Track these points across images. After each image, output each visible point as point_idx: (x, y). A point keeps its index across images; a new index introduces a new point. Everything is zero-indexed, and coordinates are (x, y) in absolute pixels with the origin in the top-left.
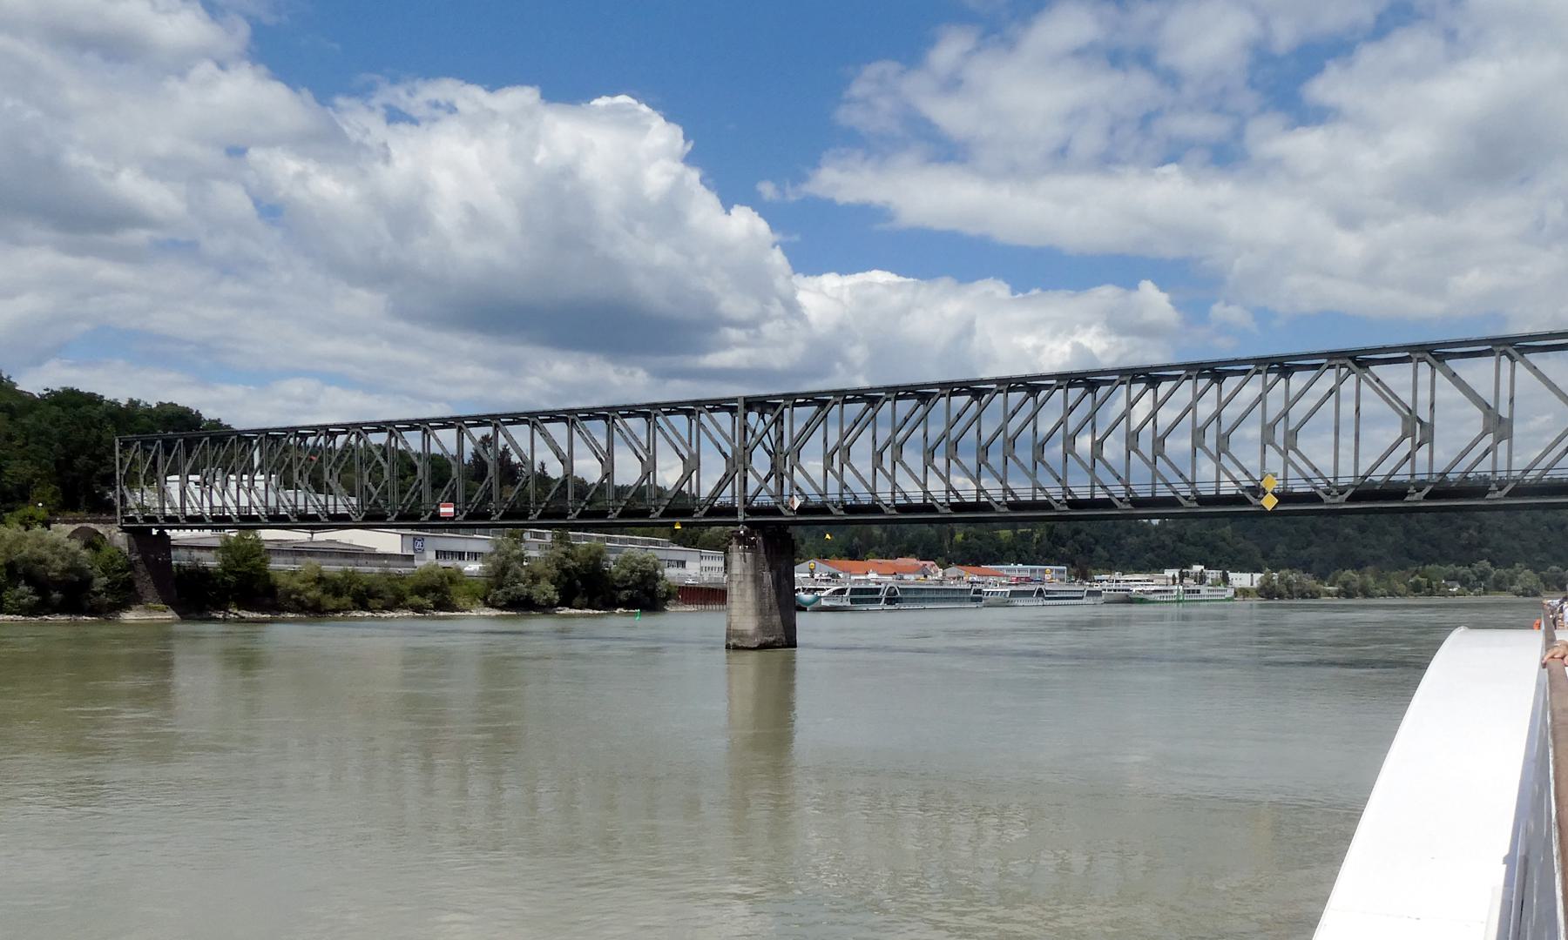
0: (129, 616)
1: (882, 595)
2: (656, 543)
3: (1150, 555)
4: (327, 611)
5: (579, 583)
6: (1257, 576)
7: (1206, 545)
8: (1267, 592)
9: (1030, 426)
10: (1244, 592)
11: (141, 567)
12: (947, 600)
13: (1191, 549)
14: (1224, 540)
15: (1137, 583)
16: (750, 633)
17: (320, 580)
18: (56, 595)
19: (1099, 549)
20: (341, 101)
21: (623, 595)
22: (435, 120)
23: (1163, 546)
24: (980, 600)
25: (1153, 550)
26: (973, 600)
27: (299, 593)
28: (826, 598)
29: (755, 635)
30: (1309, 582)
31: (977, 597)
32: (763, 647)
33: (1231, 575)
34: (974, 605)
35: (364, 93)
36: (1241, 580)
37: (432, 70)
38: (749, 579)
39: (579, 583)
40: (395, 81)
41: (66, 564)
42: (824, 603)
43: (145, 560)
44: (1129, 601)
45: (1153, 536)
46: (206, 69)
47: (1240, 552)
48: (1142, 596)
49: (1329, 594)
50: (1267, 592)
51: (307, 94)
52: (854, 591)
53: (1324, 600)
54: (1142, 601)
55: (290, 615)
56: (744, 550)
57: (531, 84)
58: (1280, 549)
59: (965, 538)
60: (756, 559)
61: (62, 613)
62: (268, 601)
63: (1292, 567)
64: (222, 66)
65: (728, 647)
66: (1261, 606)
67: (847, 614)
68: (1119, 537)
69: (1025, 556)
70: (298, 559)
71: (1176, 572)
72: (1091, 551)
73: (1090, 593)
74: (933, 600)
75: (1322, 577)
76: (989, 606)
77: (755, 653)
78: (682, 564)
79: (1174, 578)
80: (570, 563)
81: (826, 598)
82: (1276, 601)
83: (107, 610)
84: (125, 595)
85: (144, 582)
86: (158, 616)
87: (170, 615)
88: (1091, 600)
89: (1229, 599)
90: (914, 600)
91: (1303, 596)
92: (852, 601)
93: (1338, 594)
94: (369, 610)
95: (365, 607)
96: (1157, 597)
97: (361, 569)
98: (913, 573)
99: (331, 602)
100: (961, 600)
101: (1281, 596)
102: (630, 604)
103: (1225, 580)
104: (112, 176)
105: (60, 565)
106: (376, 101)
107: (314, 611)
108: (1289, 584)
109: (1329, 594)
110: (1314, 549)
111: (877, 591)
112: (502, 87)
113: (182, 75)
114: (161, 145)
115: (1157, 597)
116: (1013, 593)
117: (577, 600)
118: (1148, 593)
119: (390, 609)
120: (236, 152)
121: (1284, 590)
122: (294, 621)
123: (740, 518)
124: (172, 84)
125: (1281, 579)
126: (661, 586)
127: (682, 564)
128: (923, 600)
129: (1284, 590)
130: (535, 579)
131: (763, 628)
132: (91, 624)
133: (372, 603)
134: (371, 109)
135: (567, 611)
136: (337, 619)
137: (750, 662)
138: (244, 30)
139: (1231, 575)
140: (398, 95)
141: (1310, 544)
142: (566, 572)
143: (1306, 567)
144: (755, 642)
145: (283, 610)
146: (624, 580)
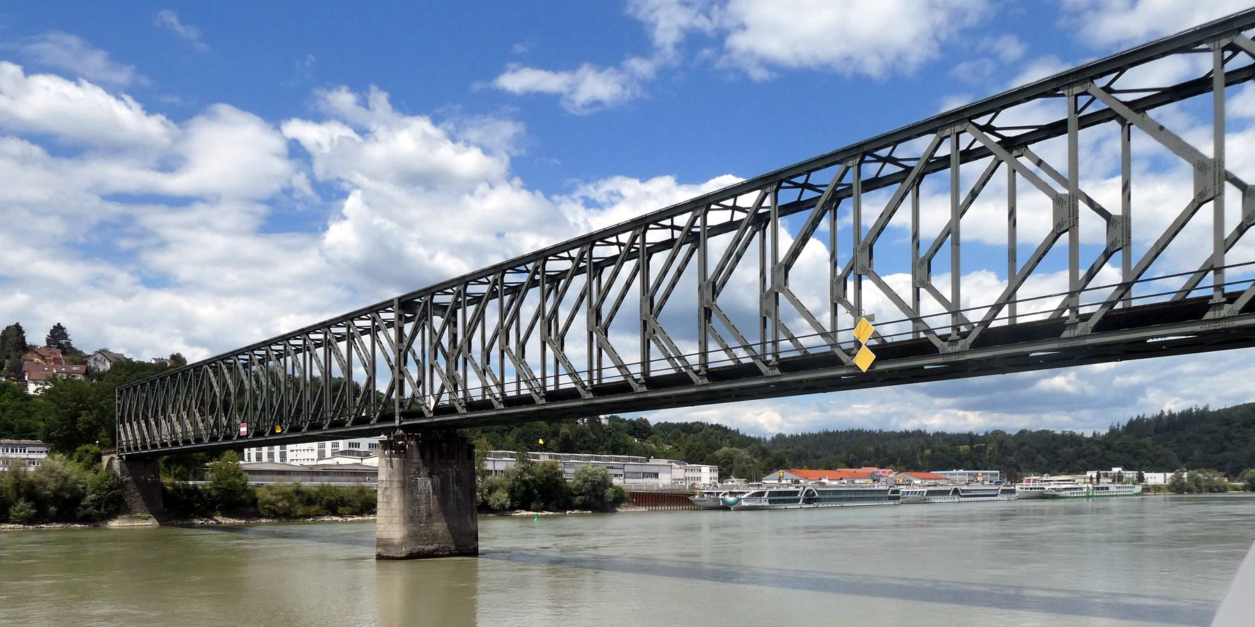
0: (114, 524)
1: (801, 496)
2: (636, 460)
3: (1082, 461)
4: (297, 517)
5: (536, 491)
6: (1169, 475)
7: (1129, 452)
8: (1177, 488)
9: (637, 282)
10: (1157, 488)
11: (132, 487)
12: (863, 499)
13: (1117, 455)
14: (1145, 447)
15: (1054, 482)
16: (396, 542)
17: (298, 492)
18: (53, 509)
19: (1040, 457)
20: (556, 198)
21: (578, 500)
22: (612, 204)
23: (1093, 454)
24: (898, 498)
25: (1084, 457)
26: (891, 498)
27: (272, 503)
28: (746, 500)
29: (403, 544)
30: (1218, 478)
31: (894, 496)
32: (411, 556)
33: (1146, 475)
34: (892, 503)
35: (568, 191)
36: (1155, 478)
37: (607, 173)
38: (396, 485)
39: (536, 491)
40: (587, 182)
41: (59, 484)
42: (744, 503)
43: (136, 481)
44: (1043, 497)
45: (1085, 445)
46: (482, 188)
47: (1158, 456)
48: (1054, 493)
49: (1236, 489)
50: (1177, 488)
51: (539, 193)
52: (771, 494)
53: (1232, 494)
54: (1054, 497)
55: (264, 521)
56: (391, 456)
57: (671, 175)
58: (1197, 454)
59: (933, 452)
60: (405, 464)
61: (58, 522)
62: (252, 510)
63: (1207, 467)
64: (491, 187)
65: (380, 557)
66: (1172, 500)
67: (766, 513)
68: (1056, 448)
69: (979, 464)
70: (315, 478)
71: (1094, 474)
72: (1033, 459)
73: (1004, 492)
74: (851, 499)
75: (1234, 473)
76: (909, 503)
77: (403, 564)
78: (656, 475)
79: (1091, 478)
80: (527, 477)
81: (746, 500)
82: (1186, 495)
83: (94, 519)
84: (114, 504)
85: (134, 497)
86: (139, 524)
87: (152, 523)
88: (1005, 497)
89: (1137, 494)
90: (831, 500)
91: (1211, 491)
92: (770, 502)
93: (1244, 489)
94: (341, 516)
95: (335, 513)
96: (1068, 493)
97: (333, 484)
98: (888, 478)
99: (300, 510)
100: (879, 499)
101: (1190, 491)
102: (584, 507)
103: (1141, 479)
104: (432, 257)
105: (52, 485)
106: (576, 195)
107: (287, 515)
108: (1197, 481)
109: (1236, 489)
110: (1228, 454)
111: (796, 493)
112: (650, 178)
113: (471, 193)
114: (460, 237)
115: (1068, 493)
116: (929, 493)
117: (533, 505)
118: (1059, 490)
119: (358, 514)
120: (500, 235)
121: (1193, 486)
122: (576, 515)
123: (397, 422)
124: (467, 199)
125: (1190, 477)
126: (609, 492)
127: (656, 475)
128: (841, 500)
129: (1193, 486)
130: (492, 489)
131: (413, 536)
132: (85, 529)
133: (340, 509)
134: (575, 201)
135: (524, 513)
136: (308, 523)
137: (399, 573)
138: (506, 159)
139: (1146, 475)
140: (591, 191)
141: (1224, 449)
142: (525, 483)
143: (1220, 467)
144: (404, 551)
145: (262, 517)
146: (578, 488)
